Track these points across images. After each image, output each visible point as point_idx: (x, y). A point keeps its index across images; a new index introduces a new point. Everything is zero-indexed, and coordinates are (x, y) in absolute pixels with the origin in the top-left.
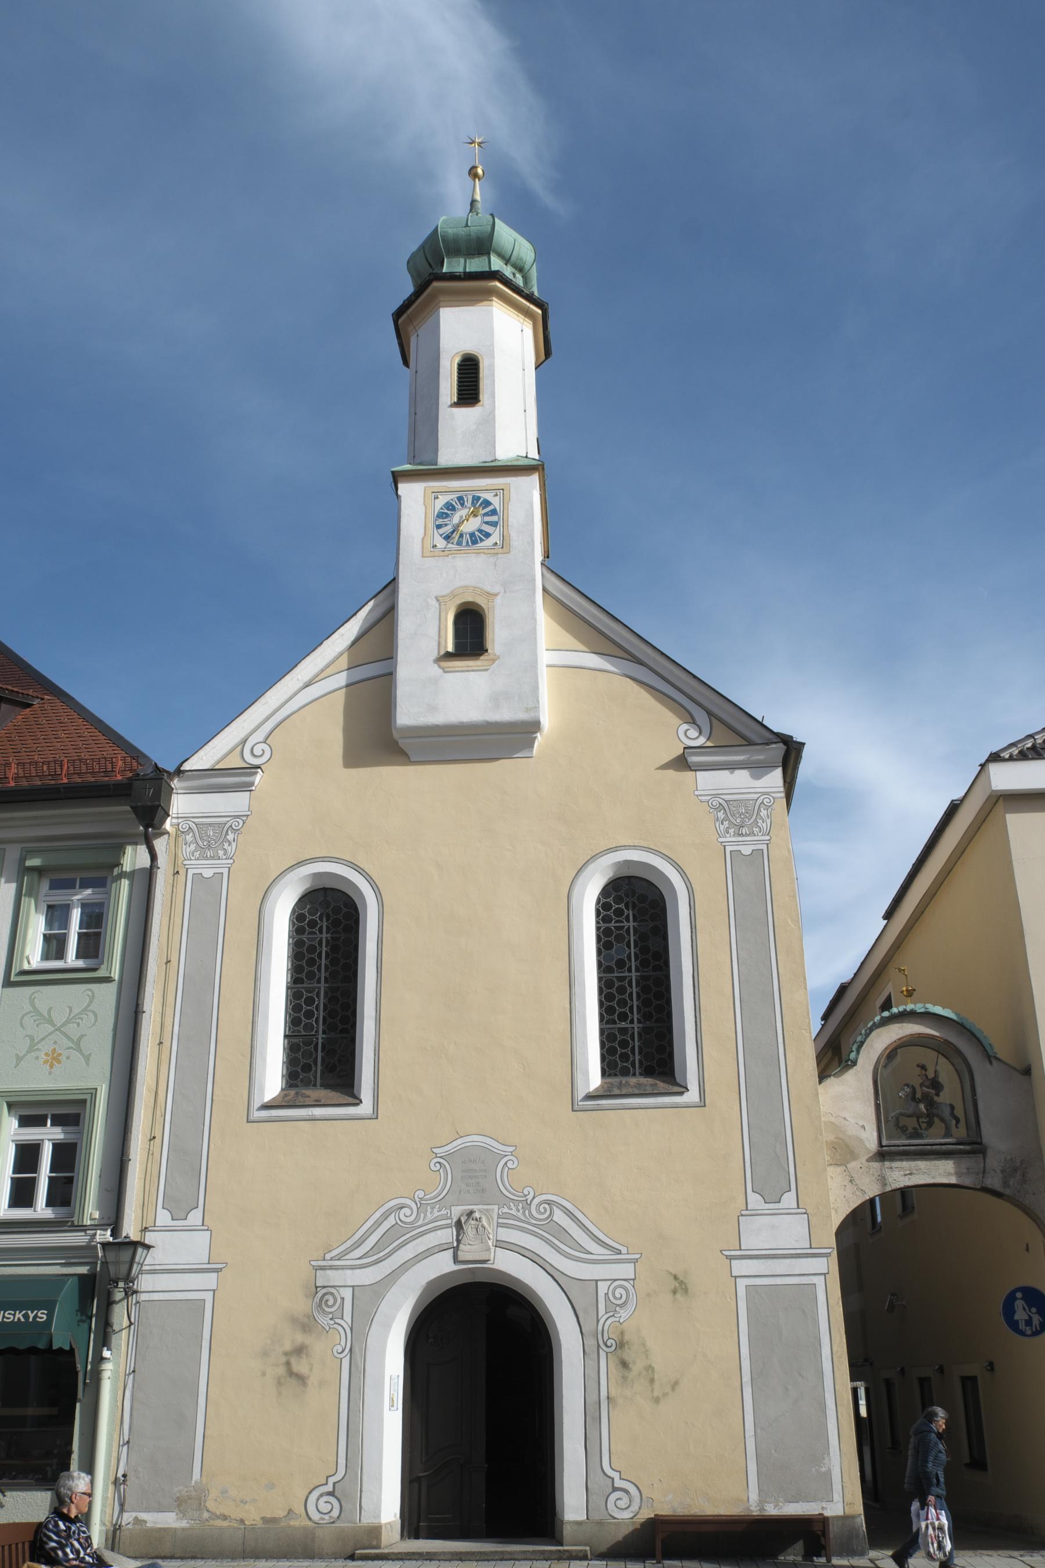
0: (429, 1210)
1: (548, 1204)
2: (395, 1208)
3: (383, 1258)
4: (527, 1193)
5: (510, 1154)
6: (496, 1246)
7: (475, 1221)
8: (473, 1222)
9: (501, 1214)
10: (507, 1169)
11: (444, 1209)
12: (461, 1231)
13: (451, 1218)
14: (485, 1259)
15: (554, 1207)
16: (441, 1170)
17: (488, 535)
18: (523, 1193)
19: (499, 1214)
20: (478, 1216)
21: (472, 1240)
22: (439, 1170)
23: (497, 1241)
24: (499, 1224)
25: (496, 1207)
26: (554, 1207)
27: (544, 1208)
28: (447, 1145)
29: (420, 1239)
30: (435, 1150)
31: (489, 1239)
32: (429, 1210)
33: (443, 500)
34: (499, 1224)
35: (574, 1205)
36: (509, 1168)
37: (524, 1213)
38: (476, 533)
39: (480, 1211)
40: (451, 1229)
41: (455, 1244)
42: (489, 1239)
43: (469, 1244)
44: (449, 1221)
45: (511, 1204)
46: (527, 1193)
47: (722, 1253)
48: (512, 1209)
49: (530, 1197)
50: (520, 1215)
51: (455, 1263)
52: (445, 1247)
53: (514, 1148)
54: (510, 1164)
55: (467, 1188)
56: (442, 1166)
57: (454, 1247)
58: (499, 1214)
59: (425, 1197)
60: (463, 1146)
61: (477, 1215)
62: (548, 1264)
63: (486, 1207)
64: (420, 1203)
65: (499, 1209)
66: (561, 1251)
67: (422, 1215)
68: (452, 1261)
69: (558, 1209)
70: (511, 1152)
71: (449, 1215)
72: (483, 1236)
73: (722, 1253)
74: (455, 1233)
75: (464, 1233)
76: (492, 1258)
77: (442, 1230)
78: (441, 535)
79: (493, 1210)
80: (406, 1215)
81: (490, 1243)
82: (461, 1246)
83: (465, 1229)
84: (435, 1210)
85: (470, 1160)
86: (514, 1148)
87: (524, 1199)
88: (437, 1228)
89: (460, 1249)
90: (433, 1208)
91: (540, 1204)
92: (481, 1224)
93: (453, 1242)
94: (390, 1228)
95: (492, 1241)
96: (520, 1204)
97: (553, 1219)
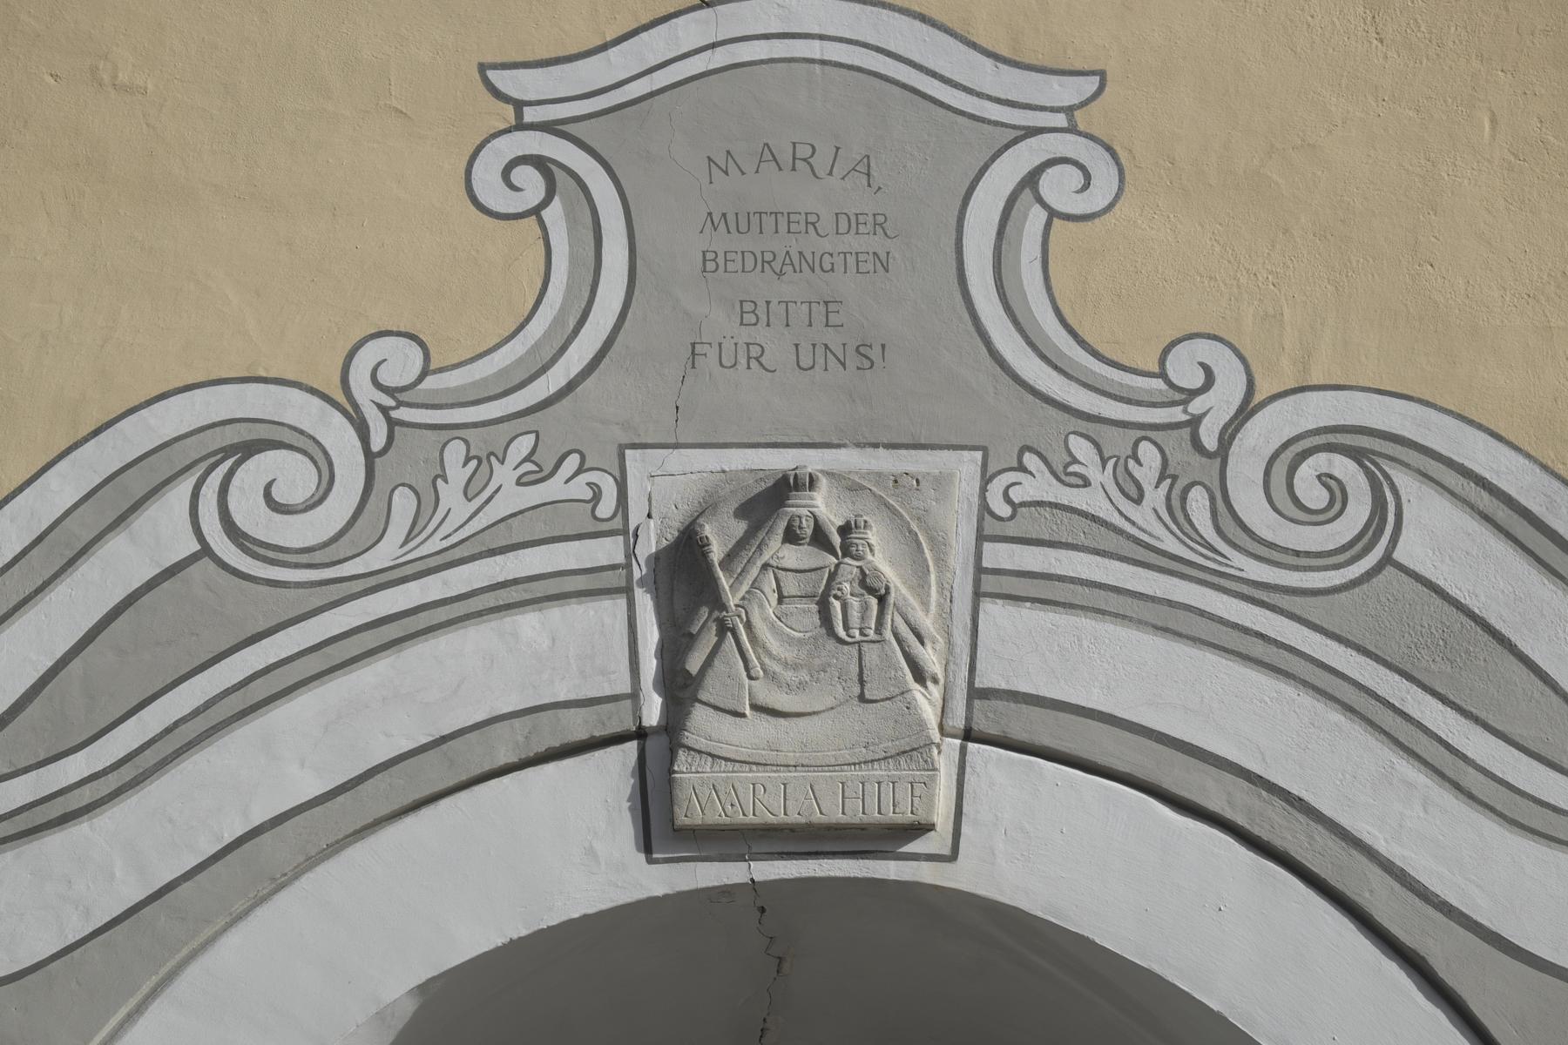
0: (458, 473)
1: (1356, 454)
2: (193, 449)
3: (86, 795)
4: (1198, 380)
5: (1060, 120)
6: (968, 735)
7: (806, 550)
8: (792, 556)
9: (1004, 510)
10: (1037, 217)
11: (572, 462)
12: (704, 612)
13: (624, 532)
14: (890, 816)
15: (1402, 479)
16: (554, 214)
18: (1163, 375)
19: (985, 508)
20: (833, 518)
21: (789, 675)
22: (536, 211)
23: (976, 694)
24: (989, 583)
25: (966, 466)
26: (1402, 479)
27: (1325, 479)
28: (604, 47)
29: (382, 666)
30: (512, 83)
31: (920, 675)
32: (458, 473)
34: (989, 583)
35: (1544, 467)
36: (1053, 214)
37: (1177, 510)
39: (850, 485)
40: (622, 602)
41: (653, 711)
42: (920, 675)
43: (755, 707)
44: (608, 551)
45: (1080, 447)
46: (1198, 380)
47: (1115, 456)
48: (1086, 483)
49: (1219, 405)
50: (1147, 518)
51: (647, 846)
52: (578, 726)
53: (1091, 84)
54: (1059, 188)
55: (744, 335)
56: (559, 175)
57: (641, 734)
58: (985, 508)
59: (430, 382)
60: (719, 58)
61: (825, 506)
62: (1375, 872)
63: (886, 462)
64: (392, 424)
65: (986, 480)
66: (1471, 779)
67: (404, 504)
68: (627, 830)
69: (1429, 492)
70: (1069, 110)
71: (606, 507)
72: (872, 655)
73: (1115, 456)
74: (650, 635)
75: (724, 629)
76: (942, 814)
77: (555, 613)
79: (942, 482)
80: (278, 495)
81: (926, 703)
82: (703, 724)
83: (732, 601)
84: (505, 475)
85: (768, 154)
86: (1091, 84)
87: (1177, 414)
88: (514, 595)
89: (690, 738)
90: (483, 461)
91: (1296, 451)
92: (850, 567)
93: (635, 696)
94: (151, 585)
95: (936, 692)
96: (1147, 451)
97: (1398, 555)
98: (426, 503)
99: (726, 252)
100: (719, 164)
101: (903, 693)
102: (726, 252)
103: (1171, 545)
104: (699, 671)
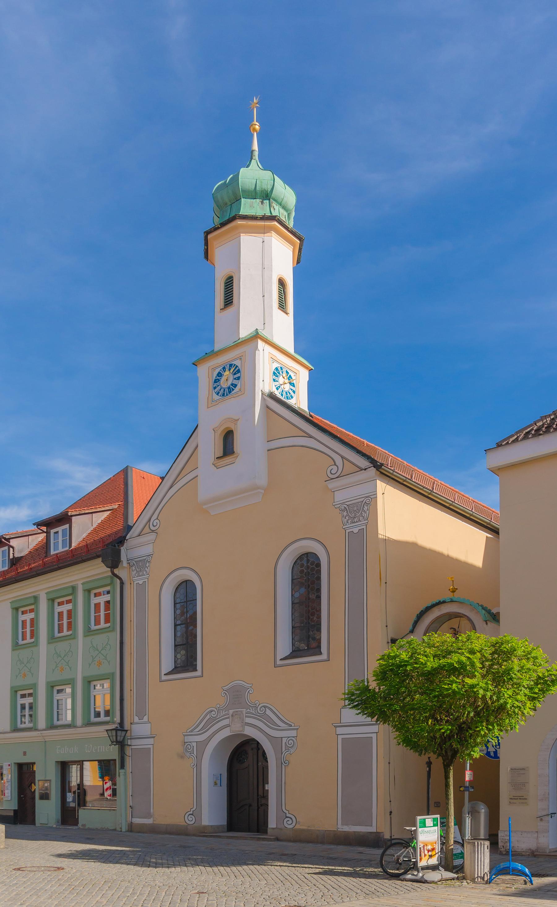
32: (221, 712)
37: (255, 711)
38: (231, 386)
50: (254, 712)
54: (250, 692)
78: (216, 393)
90: (222, 711)
98: (220, 714)
99: (329, 660)
102: (329, 660)
104: (255, 353)
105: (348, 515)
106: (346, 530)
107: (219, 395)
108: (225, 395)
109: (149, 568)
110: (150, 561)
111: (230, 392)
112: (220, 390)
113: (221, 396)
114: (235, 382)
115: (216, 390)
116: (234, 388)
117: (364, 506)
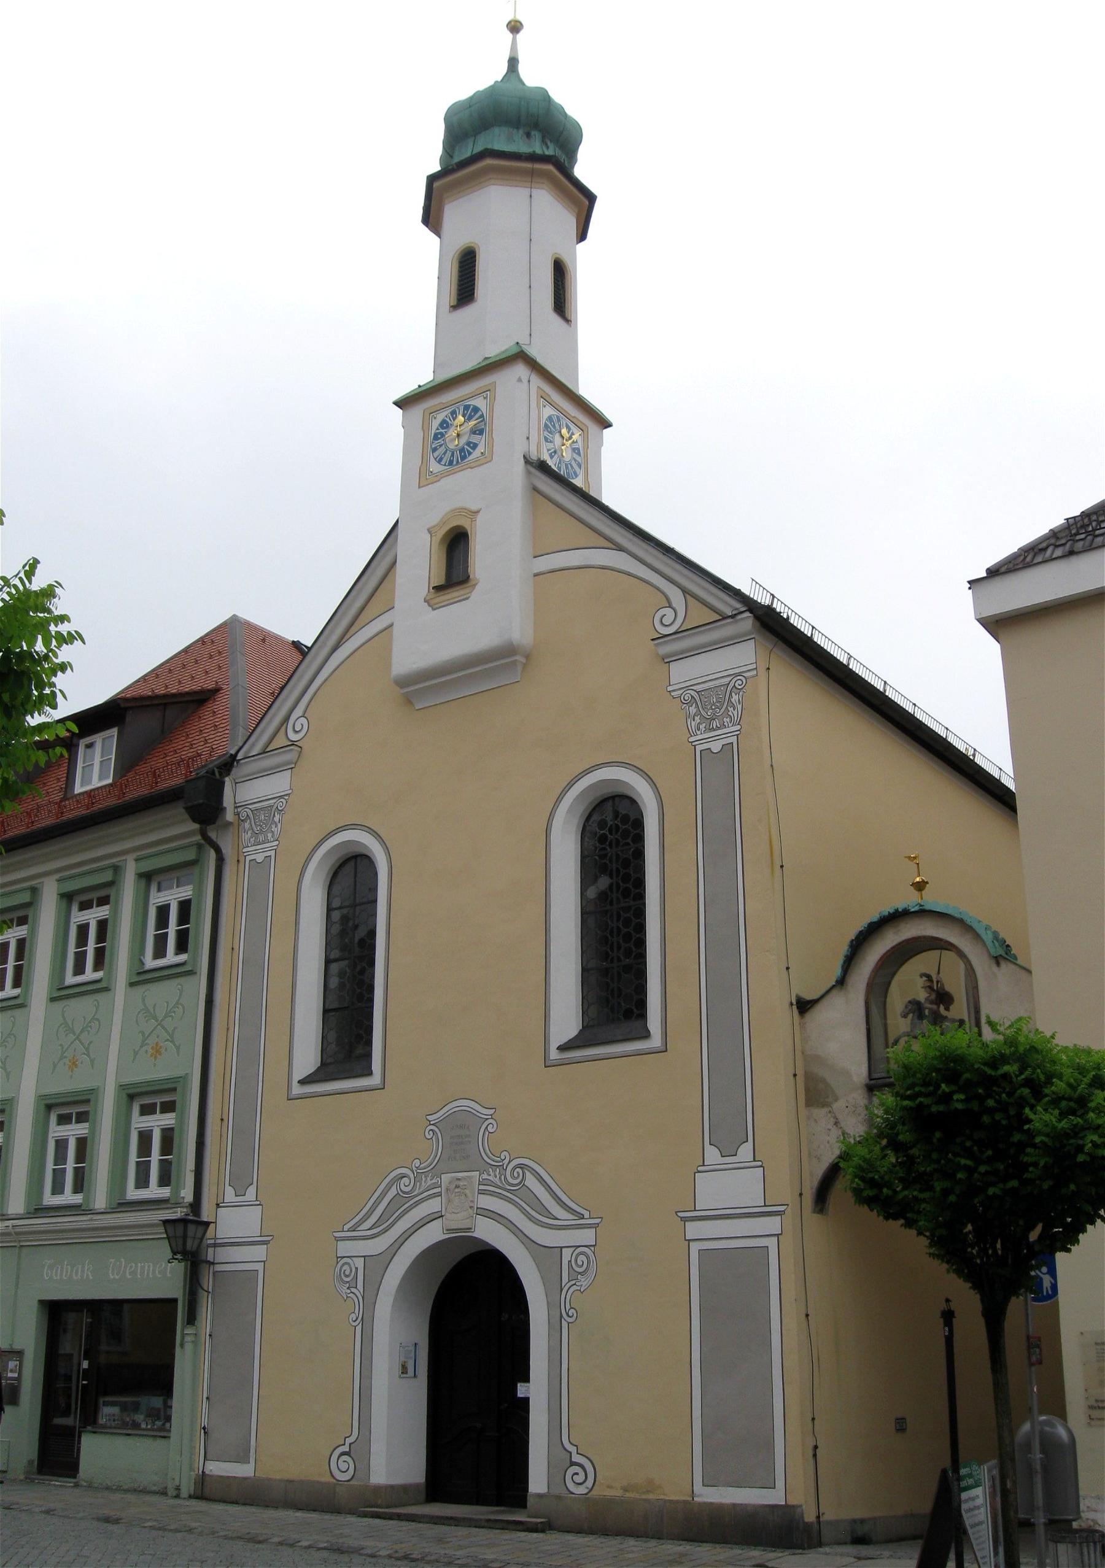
5: (490, 1117)
10: (487, 1133)
15: (526, 1171)
17: (475, 446)
26: (526, 1171)
33: (441, 417)
45: (490, 1170)
49: (506, 1161)
50: (497, 1180)
54: (490, 1129)
64: (417, 1173)
67: (418, 1184)
70: (491, 1115)
87: (501, 1164)
96: (498, 1170)
100: (717, 619)
101: (190, 1530)
103: (499, 1184)
105: (698, 713)
106: (695, 746)
107: (443, 463)
108: (455, 463)
109: (279, 825)
110: (282, 810)
111: (463, 458)
112: (445, 453)
113: (445, 465)
114: (475, 439)
115: (436, 454)
116: (472, 451)
117: (731, 694)
